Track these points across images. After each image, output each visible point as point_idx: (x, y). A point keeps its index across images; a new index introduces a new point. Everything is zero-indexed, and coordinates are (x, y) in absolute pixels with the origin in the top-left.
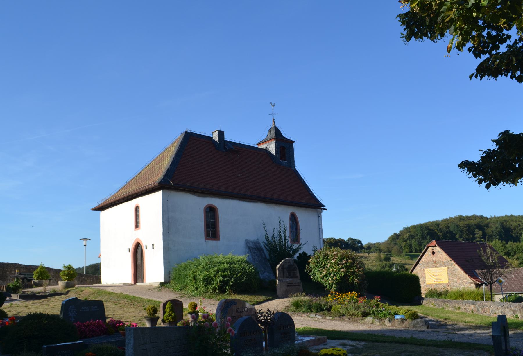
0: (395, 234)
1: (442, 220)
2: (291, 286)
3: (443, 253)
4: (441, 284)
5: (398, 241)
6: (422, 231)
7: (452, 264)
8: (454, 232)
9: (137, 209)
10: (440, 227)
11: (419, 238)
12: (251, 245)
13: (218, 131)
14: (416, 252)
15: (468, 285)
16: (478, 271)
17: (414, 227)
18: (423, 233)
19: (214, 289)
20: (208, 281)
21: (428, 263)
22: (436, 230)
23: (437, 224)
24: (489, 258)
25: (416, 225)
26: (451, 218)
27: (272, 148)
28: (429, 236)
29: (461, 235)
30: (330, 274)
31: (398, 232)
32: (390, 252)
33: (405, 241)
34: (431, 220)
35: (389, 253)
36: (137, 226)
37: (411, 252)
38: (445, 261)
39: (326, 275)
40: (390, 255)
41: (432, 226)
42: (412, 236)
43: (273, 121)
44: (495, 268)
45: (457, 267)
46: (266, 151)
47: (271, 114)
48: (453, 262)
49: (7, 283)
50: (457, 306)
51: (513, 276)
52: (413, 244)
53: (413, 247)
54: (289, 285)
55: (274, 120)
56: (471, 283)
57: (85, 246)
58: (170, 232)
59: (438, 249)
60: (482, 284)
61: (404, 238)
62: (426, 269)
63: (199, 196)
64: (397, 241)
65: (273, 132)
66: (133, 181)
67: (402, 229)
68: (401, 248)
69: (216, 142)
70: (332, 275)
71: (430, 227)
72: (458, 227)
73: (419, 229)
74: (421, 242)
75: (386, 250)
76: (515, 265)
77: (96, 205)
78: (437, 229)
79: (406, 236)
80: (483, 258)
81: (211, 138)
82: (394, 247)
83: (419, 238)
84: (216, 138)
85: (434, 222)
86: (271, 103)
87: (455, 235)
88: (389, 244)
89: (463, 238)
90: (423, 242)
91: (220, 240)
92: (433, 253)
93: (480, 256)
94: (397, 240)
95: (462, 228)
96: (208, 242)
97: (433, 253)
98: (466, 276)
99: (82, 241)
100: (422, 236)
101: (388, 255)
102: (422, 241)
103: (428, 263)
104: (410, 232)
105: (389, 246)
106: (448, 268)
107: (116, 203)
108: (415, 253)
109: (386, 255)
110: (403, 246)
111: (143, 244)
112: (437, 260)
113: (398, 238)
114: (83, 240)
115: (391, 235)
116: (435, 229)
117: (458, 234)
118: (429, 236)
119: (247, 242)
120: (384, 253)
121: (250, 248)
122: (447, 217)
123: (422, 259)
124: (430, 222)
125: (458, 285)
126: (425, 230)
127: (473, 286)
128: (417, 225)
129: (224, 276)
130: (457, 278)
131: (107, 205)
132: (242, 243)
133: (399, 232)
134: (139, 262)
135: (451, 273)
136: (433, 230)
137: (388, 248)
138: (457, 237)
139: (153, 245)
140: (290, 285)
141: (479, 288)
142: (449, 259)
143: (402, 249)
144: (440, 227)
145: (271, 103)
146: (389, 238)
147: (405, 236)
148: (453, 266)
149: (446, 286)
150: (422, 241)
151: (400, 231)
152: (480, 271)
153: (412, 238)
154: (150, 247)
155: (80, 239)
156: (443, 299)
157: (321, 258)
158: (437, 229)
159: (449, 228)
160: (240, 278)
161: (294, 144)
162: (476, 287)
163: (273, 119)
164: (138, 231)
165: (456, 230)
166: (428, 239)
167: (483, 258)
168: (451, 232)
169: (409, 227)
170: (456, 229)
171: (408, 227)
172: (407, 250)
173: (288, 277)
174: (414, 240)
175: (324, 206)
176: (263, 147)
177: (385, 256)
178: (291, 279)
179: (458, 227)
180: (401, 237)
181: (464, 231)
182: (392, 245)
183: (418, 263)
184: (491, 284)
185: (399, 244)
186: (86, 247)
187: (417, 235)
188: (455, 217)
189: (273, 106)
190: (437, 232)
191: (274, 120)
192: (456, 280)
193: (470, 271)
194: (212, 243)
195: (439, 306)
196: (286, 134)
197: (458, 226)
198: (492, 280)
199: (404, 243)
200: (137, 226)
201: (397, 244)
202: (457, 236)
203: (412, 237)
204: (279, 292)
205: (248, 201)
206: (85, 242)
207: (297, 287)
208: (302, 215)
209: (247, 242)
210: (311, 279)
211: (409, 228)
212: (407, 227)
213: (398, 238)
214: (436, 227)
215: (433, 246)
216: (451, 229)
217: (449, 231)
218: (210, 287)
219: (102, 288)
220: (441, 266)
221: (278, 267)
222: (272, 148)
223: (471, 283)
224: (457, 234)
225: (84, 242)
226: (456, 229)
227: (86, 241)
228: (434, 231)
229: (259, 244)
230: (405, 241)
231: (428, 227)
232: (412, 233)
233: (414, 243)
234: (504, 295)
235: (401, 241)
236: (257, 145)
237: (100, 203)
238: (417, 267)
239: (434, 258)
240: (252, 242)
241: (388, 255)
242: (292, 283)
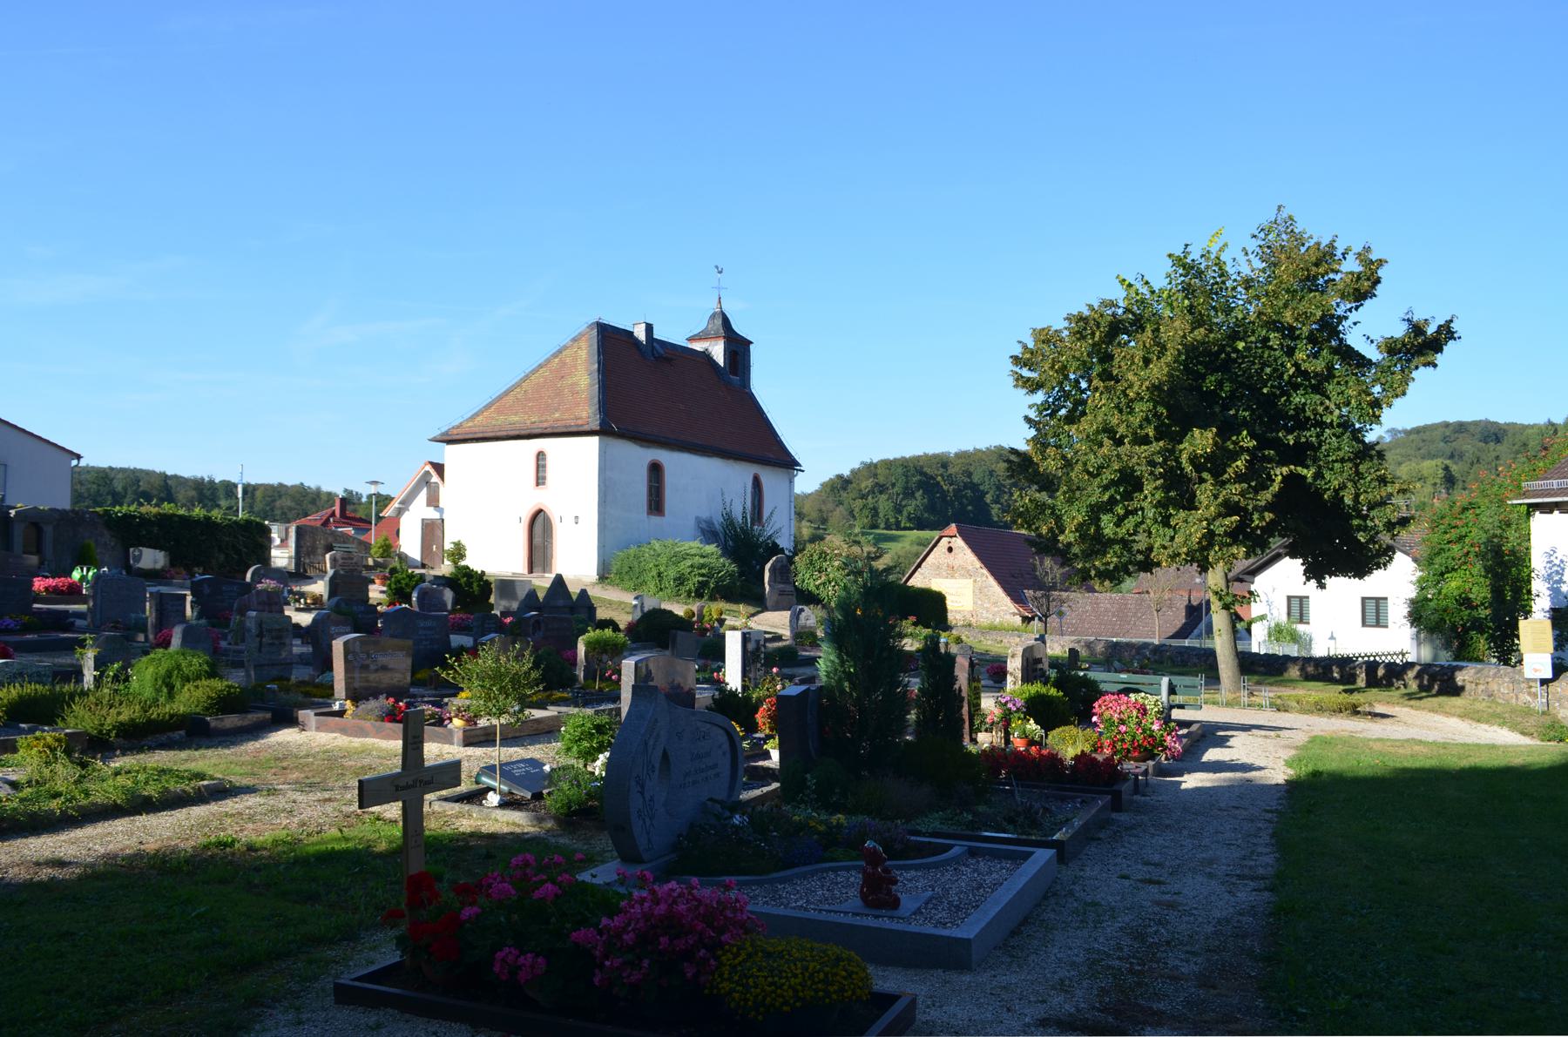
0: (840, 477)
1: (956, 454)
3: (968, 552)
4: (959, 612)
5: (845, 495)
6: (907, 476)
7: (983, 574)
8: (982, 488)
9: (541, 456)
10: (951, 470)
11: (898, 494)
12: (704, 525)
14: (888, 527)
15: (1008, 617)
16: (1029, 593)
17: (888, 464)
18: (907, 482)
19: (689, 593)
20: (680, 580)
21: (938, 567)
22: (939, 478)
23: (943, 462)
24: (1047, 573)
25: (891, 458)
26: (977, 451)
27: (718, 351)
28: (921, 491)
29: (998, 496)
30: (830, 583)
31: (846, 473)
32: (824, 521)
33: (862, 498)
34: (931, 451)
35: (823, 524)
36: (540, 480)
37: (875, 526)
38: (970, 568)
39: (824, 584)
40: (825, 529)
41: (930, 467)
42: (882, 486)
43: (717, 300)
44: (1055, 590)
45: (991, 581)
46: (706, 357)
48: (985, 571)
50: (999, 639)
51: (1089, 608)
52: (881, 507)
53: (881, 515)
56: (1014, 614)
59: (959, 542)
60: (1033, 619)
61: (861, 490)
62: (933, 580)
63: (642, 446)
64: (844, 495)
65: (719, 322)
66: (510, 399)
67: (857, 466)
68: (851, 513)
69: (640, 342)
70: (833, 584)
71: (925, 469)
72: (992, 476)
73: (900, 470)
74: (900, 505)
75: (814, 515)
76: (1491, 449)
78: (942, 475)
79: (867, 484)
80: (1038, 573)
81: (630, 334)
82: (835, 510)
83: (898, 494)
84: (640, 334)
85: (935, 456)
86: (717, 267)
87: (984, 493)
88: (824, 502)
89: (1002, 504)
90: (905, 506)
92: (950, 550)
93: (1034, 569)
94: (842, 492)
95: (1001, 479)
97: (950, 550)
98: (1007, 600)
100: (906, 488)
101: (819, 528)
102: (903, 503)
103: (938, 567)
104: (875, 475)
105: (824, 508)
106: (975, 581)
108: (885, 532)
109: (815, 528)
110: (857, 510)
111: (554, 513)
112: (956, 563)
113: (845, 489)
115: (828, 479)
116: (937, 475)
117: (991, 492)
118: (921, 491)
119: (698, 520)
120: (808, 524)
121: (703, 532)
122: (968, 446)
123: (928, 559)
124: (926, 455)
125: (991, 616)
126: (913, 475)
127: (1018, 620)
128: (895, 460)
129: (703, 575)
130: (989, 602)
132: (692, 522)
133: (848, 473)
134: (537, 540)
135: (980, 591)
136: (932, 477)
137: (820, 511)
138: (988, 501)
139: (577, 517)
140: (782, 593)
141: (1029, 623)
142: (978, 564)
143: (854, 517)
144: (951, 470)
145: (717, 267)
146: (824, 485)
147: (863, 485)
148: (984, 579)
149: (968, 616)
150: (903, 503)
151: (852, 471)
152: (1031, 592)
153: (881, 493)
154: (569, 520)
157: (816, 557)
158: (942, 475)
159: (970, 475)
160: (721, 579)
161: (751, 346)
162: (1023, 621)
164: (541, 490)
165: (987, 483)
166: (919, 498)
167: (1038, 573)
168: (974, 487)
169: (875, 461)
170: (986, 479)
171: (871, 463)
172: (866, 521)
174: (884, 497)
175: (799, 465)
176: (698, 346)
177: (811, 530)
179: (992, 476)
180: (854, 485)
181: (1005, 487)
182: (830, 506)
183: (919, 566)
184: (1046, 616)
185: (846, 502)
187: (893, 485)
188: (987, 449)
189: (720, 272)
190: (942, 483)
192: (988, 605)
193: (1015, 593)
194: (655, 519)
195: (975, 638)
196: (739, 328)
197: (991, 473)
198: (1048, 610)
199: (859, 503)
200: (540, 480)
201: (841, 503)
202: (988, 498)
203: (881, 488)
204: (769, 603)
205: (701, 455)
208: (770, 478)
209: (698, 520)
211: (876, 466)
212: (869, 461)
213: (845, 489)
214: (942, 470)
215: (951, 537)
216: (976, 479)
217: (971, 482)
218: (683, 589)
220: (963, 576)
221: (768, 566)
222: (718, 351)
223: (1014, 614)
224: (987, 493)
226: (986, 479)
228: (935, 479)
229: (713, 524)
230: (863, 497)
231: (922, 467)
232: (881, 480)
233: (884, 504)
234: (1267, 881)
235: (852, 495)
236: (691, 339)
238: (917, 574)
239: (950, 558)
240: (705, 521)
241: (819, 528)
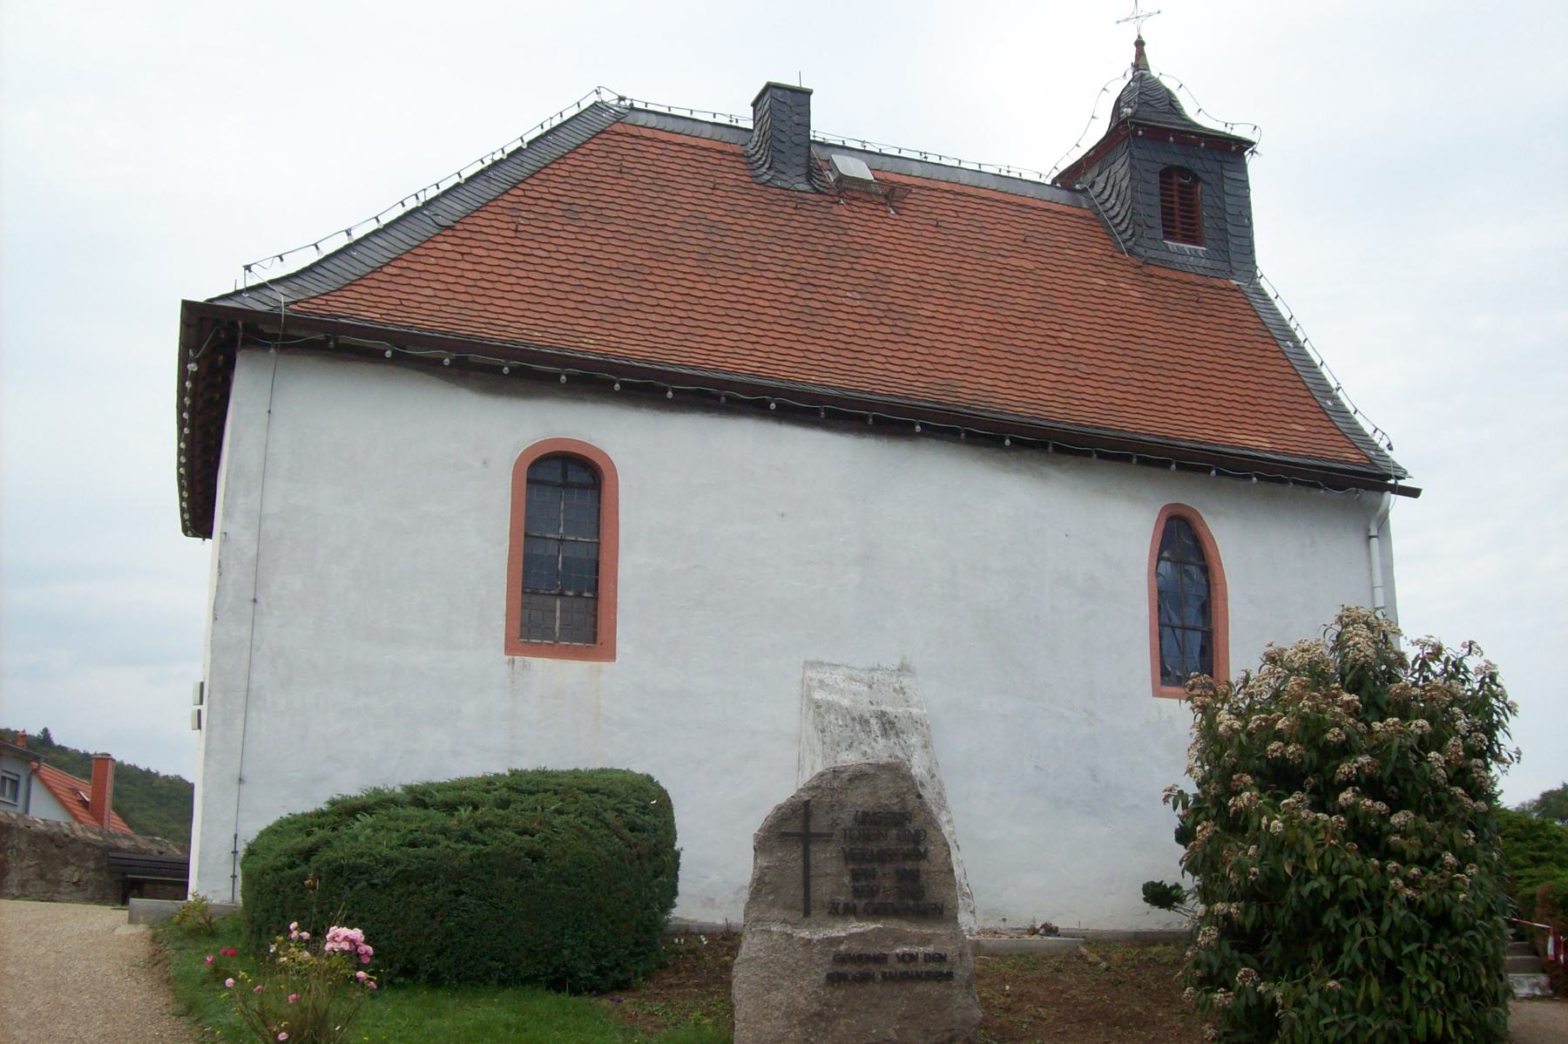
2: (865, 978)
54: (851, 969)
58: (262, 600)
91: (1156, 699)
96: (525, 666)
173: (848, 912)
178: (872, 926)
207: (920, 988)
242: (881, 959)
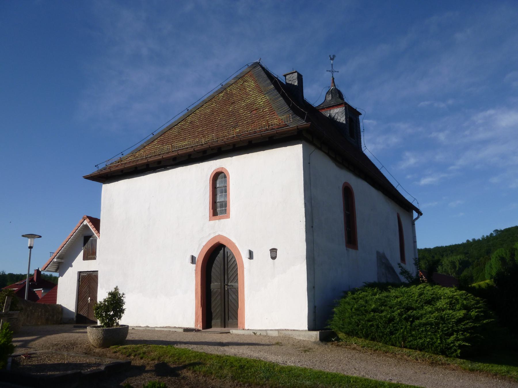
13: (297, 73)
47: (329, 71)
49: (159, 383)
55: (333, 79)
57: (31, 247)
77: (92, 170)
99: (26, 238)
107: (151, 166)
114: (29, 237)
131: (122, 171)
155: (23, 236)
156: (353, 324)
161: (360, 117)
163: (332, 79)
186: (32, 249)
191: (333, 79)
194: (352, 252)
206: (31, 241)
210: (475, 318)
219: (231, 351)
225: (29, 242)
227: (32, 239)
237: (101, 167)
